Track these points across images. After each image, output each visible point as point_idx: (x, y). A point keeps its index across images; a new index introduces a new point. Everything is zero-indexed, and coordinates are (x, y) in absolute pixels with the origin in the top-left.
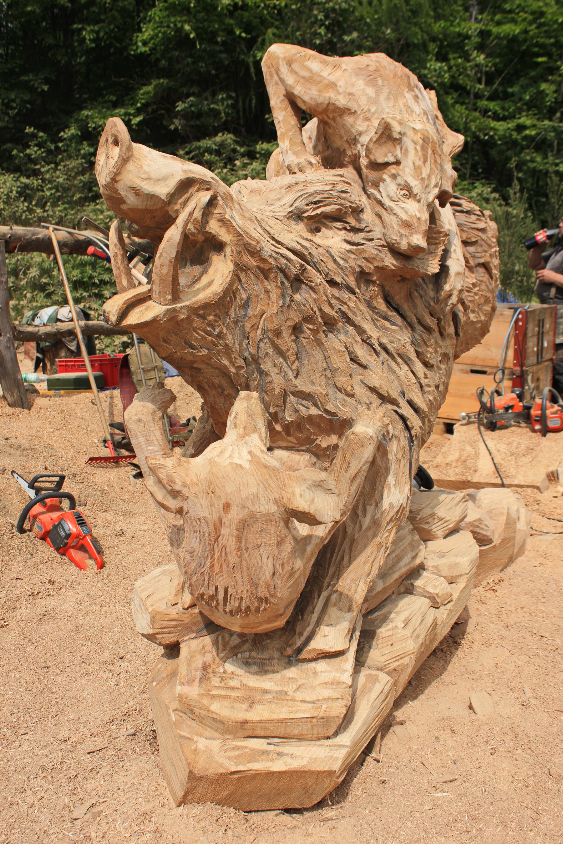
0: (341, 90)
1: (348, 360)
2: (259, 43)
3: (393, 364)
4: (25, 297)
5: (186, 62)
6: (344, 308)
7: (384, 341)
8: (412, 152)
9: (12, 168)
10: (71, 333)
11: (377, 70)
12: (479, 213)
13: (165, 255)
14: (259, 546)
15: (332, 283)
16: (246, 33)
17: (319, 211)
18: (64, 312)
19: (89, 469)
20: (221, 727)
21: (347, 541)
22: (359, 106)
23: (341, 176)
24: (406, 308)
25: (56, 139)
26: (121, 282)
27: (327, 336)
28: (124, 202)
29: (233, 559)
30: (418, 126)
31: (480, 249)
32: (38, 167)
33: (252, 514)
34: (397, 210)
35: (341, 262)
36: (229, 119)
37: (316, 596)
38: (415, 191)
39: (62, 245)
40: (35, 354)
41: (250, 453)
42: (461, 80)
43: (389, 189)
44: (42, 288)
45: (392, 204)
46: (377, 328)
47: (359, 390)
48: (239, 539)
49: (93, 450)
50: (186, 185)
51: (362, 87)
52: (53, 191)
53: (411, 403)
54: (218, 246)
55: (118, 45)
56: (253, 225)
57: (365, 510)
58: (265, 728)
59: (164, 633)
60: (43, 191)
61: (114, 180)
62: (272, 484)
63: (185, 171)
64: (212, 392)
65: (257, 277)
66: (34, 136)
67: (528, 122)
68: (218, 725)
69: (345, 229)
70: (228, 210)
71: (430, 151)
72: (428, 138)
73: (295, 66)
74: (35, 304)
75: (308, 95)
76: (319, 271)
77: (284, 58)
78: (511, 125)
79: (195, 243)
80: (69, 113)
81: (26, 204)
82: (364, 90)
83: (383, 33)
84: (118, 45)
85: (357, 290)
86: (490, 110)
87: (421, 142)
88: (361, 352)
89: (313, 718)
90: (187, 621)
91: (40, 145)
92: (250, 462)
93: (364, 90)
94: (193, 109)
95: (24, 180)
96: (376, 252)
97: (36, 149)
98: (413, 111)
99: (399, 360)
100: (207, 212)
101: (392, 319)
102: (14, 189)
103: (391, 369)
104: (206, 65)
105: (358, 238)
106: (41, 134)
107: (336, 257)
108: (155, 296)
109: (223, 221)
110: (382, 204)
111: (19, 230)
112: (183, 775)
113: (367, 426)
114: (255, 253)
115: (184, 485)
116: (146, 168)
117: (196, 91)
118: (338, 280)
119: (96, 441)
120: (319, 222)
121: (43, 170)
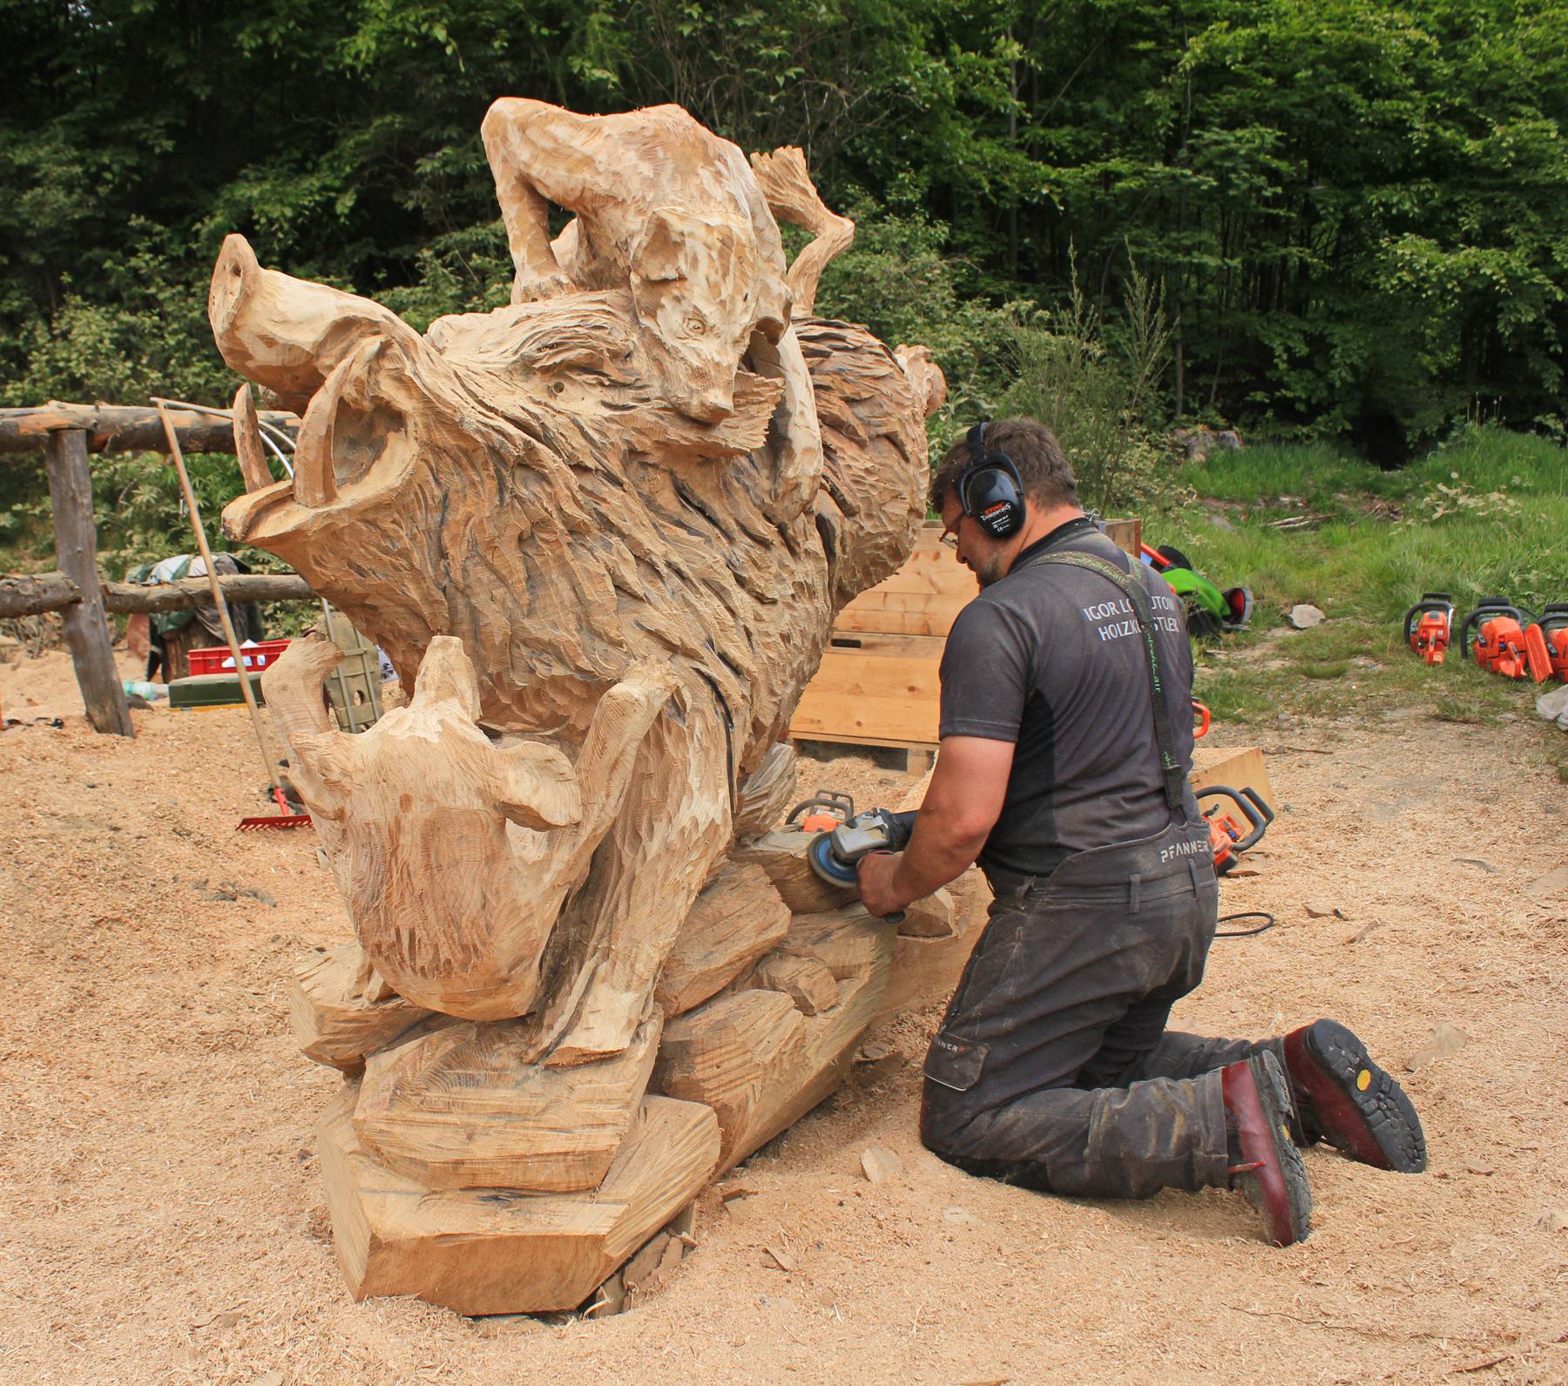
0: (601, 168)
1: (612, 589)
2: (573, 43)
3: (691, 597)
4: (131, 543)
5: (432, 82)
6: (603, 508)
7: (675, 558)
8: (704, 263)
9: (103, 294)
10: (208, 597)
11: (655, 136)
12: (881, 351)
13: (310, 432)
14: (457, 862)
15: (579, 468)
16: (546, 26)
17: (558, 359)
18: (199, 565)
19: (241, 838)
20: (423, 1172)
21: (624, 879)
22: (629, 191)
23: (603, 302)
24: (716, 507)
25: (189, 235)
26: (250, 478)
27: (574, 552)
28: (250, 357)
29: (420, 882)
30: (715, 221)
31: (877, 412)
32: (153, 290)
33: (442, 811)
34: (685, 352)
35: (596, 437)
36: (410, 228)
37: (577, 965)
38: (711, 321)
39: (184, 436)
40: (147, 647)
41: (441, 722)
42: (977, 91)
43: (669, 321)
44: (165, 524)
45: (677, 343)
46: (664, 538)
47: (632, 637)
48: (426, 850)
49: (249, 806)
50: (345, 327)
51: (634, 161)
52: (181, 337)
53: (724, 657)
54: (397, 419)
55: (304, 55)
56: (449, 384)
57: (651, 828)
58: (493, 1173)
59: (338, 1042)
60: (162, 337)
61: (234, 326)
62: (474, 767)
63: (341, 308)
64: (401, 646)
65: (457, 462)
66: (145, 232)
67: (1124, 168)
68: (418, 1169)
69: (602, 384)
70: (408, 364)
71: (733, 259)
72: (731, 238)
73: (532, 133)
74: (147, 555)
75: (556, 180)
76: (557, 452)
77: (515, 121)
78: (1091, 170)
79: (360, 413)
80: (212, 188)
81: (129, 364)
82: (636, 166)
83: (814, 13)
84: (304, 55)
85: (625, 479)
86: (1051, 147)
87: (719, 244)
88: (632, 576)
89: (566, 1153)
90: (375, 1021)
91: (155, 250)
92: (441, 734)
93: (636, 166)
94: (448, 170)
95: (125, 317)
96: (655, 419)
97: (148, 257)
98: (710, 197)
99: (703, 589)
100: (375, 366)
101: (693, 524)
102: (107, 335)
103: (688, 604)
104: (472, 84)
105: (625, 397)
106: (159, 228)
107: (587, 429)
108: (299, 494)
109: (400, 379)
110: (660, 344)
111: (110, 411)
112: (363, 1246)
113: (641, 686)
114: (455, 427)
115: (345, 773)
116: (280, 306)
117: (455, 135)
118: (591, 463)
119: (256, 791)
120: (561, 375)
121: (161, 296)
